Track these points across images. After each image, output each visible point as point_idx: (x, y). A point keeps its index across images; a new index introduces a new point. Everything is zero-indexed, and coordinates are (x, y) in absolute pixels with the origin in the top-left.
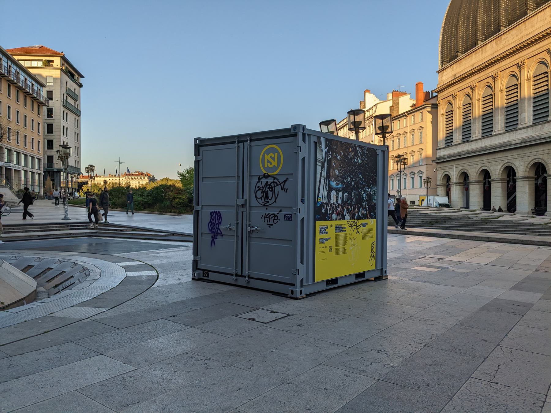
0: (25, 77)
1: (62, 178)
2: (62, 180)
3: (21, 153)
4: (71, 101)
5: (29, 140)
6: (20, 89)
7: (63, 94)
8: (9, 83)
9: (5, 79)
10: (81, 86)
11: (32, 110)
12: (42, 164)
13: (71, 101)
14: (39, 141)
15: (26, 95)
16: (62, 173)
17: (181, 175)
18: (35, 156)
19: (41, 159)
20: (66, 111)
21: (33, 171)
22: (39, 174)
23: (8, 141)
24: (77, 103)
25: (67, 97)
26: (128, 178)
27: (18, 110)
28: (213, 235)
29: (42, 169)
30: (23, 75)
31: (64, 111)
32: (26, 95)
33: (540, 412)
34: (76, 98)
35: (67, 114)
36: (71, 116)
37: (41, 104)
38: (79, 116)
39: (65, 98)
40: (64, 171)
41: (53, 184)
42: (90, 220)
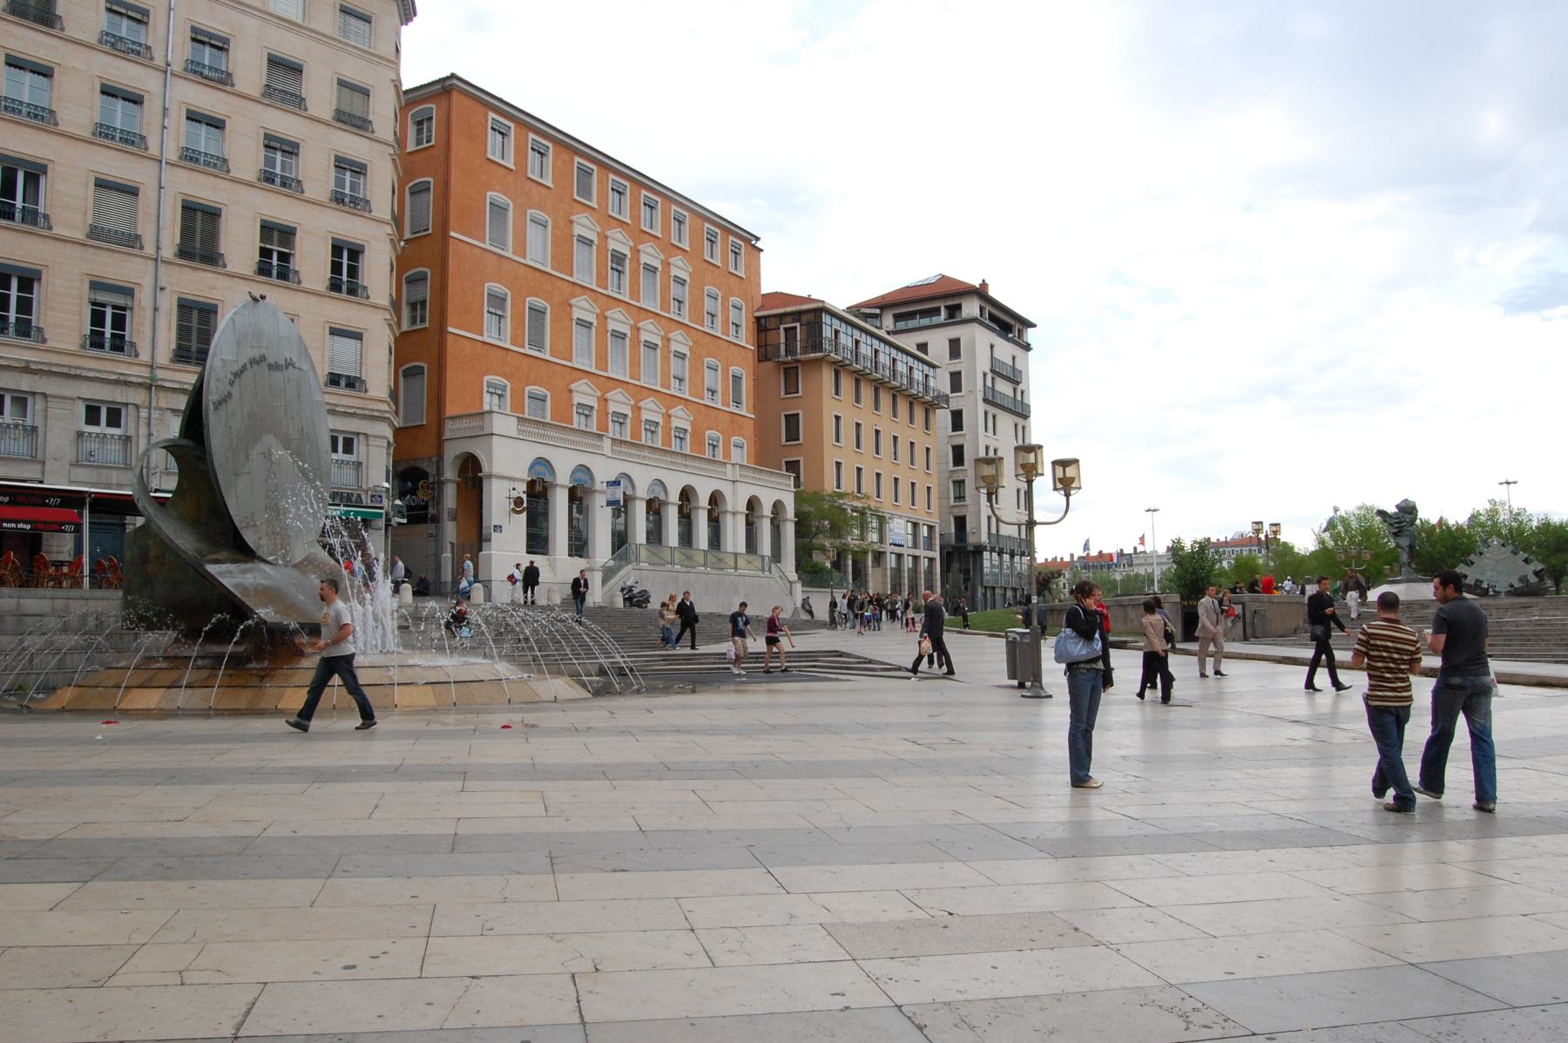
0: (925, 372)
1: (985, 566)
2: (985, 570)
3: (921, 523)
4: (1004, 387)
5: (904, 488)
6: (931, 405)
7: (985, 375)
8: (895, 393)
9: (903, 394)
10: (1027, 348)
11: (927, 429)
12: (937, 536)
13: (1004, 387)
14: (929, 488)
15: (840, 368)
16: (986, 555)
17: (1397, 506)
18: (884, 515)
19: (934, 526)
20: (992, 410)
21: (916, 554)
22: (931, 560)
23: (895, 503)
24: (1020, 387)
25: (993, 379)
26: (705, 342)
27: (837, 414)
28: (1063, 492)
29: (938, 548)
30: (849, 332)
31: (986, 413)
32: (840, 368)
33: (3, 146)
34: (1014, 377)
35: (994, 417)
36: (1006, 422)
37: (930, 407)
38: (1026, 417)
39: (989, 383)
40: (988, 548)
41: (966, 580)
42: (1336, 673)
